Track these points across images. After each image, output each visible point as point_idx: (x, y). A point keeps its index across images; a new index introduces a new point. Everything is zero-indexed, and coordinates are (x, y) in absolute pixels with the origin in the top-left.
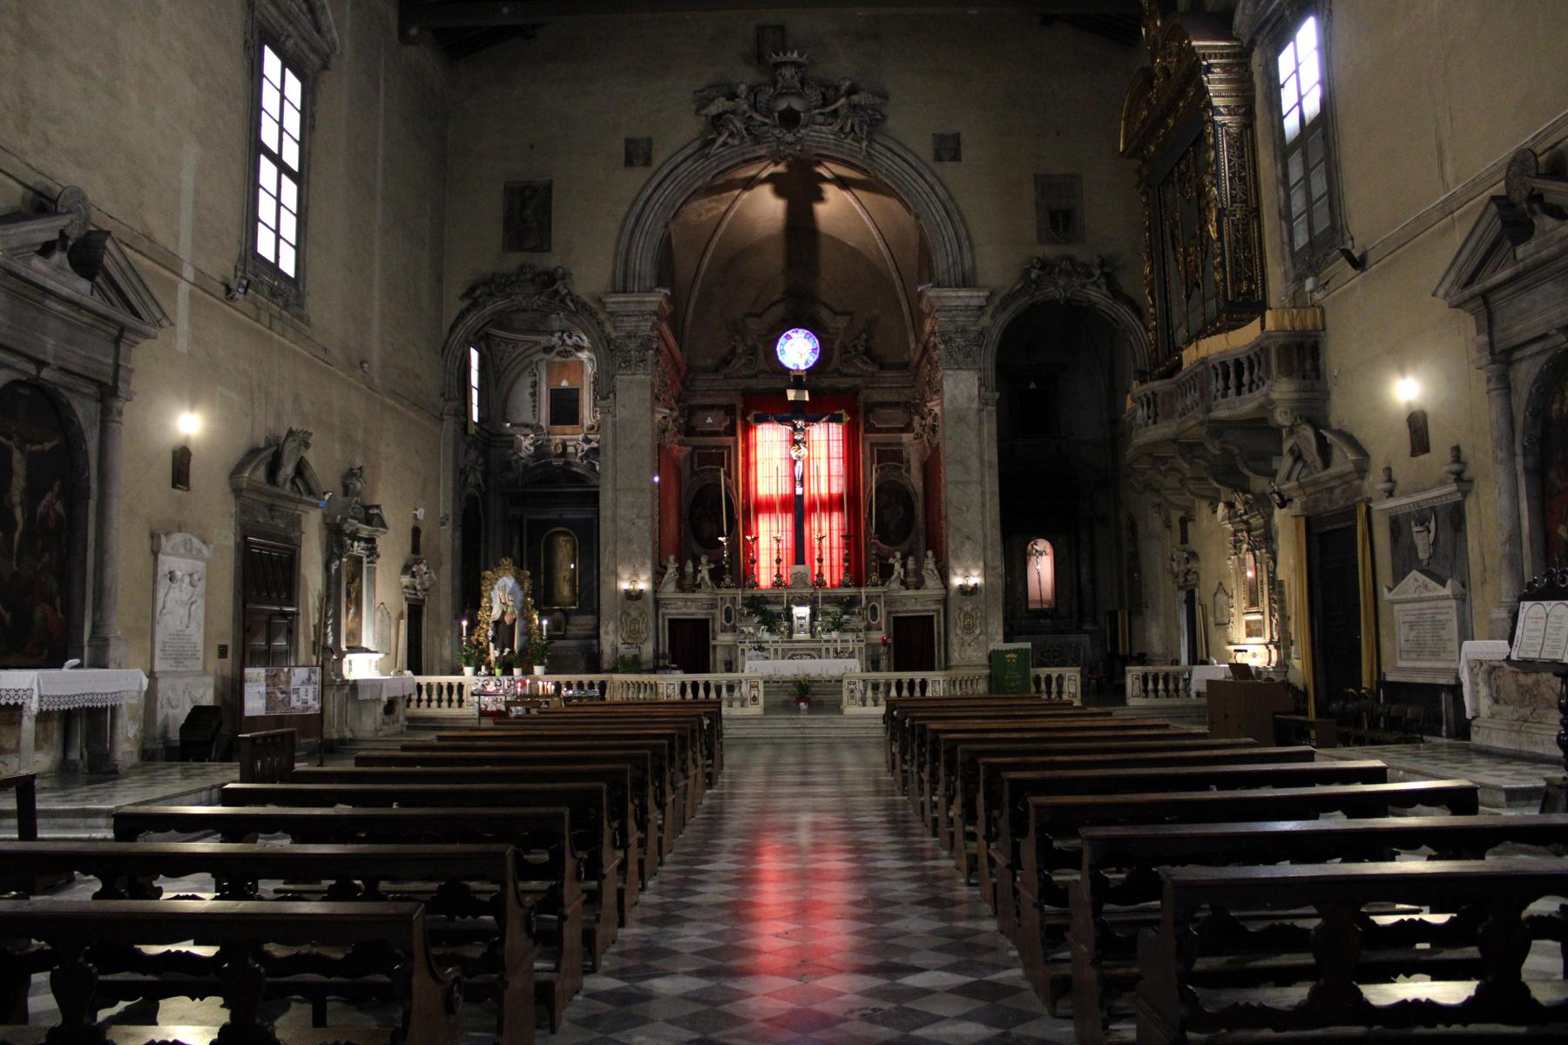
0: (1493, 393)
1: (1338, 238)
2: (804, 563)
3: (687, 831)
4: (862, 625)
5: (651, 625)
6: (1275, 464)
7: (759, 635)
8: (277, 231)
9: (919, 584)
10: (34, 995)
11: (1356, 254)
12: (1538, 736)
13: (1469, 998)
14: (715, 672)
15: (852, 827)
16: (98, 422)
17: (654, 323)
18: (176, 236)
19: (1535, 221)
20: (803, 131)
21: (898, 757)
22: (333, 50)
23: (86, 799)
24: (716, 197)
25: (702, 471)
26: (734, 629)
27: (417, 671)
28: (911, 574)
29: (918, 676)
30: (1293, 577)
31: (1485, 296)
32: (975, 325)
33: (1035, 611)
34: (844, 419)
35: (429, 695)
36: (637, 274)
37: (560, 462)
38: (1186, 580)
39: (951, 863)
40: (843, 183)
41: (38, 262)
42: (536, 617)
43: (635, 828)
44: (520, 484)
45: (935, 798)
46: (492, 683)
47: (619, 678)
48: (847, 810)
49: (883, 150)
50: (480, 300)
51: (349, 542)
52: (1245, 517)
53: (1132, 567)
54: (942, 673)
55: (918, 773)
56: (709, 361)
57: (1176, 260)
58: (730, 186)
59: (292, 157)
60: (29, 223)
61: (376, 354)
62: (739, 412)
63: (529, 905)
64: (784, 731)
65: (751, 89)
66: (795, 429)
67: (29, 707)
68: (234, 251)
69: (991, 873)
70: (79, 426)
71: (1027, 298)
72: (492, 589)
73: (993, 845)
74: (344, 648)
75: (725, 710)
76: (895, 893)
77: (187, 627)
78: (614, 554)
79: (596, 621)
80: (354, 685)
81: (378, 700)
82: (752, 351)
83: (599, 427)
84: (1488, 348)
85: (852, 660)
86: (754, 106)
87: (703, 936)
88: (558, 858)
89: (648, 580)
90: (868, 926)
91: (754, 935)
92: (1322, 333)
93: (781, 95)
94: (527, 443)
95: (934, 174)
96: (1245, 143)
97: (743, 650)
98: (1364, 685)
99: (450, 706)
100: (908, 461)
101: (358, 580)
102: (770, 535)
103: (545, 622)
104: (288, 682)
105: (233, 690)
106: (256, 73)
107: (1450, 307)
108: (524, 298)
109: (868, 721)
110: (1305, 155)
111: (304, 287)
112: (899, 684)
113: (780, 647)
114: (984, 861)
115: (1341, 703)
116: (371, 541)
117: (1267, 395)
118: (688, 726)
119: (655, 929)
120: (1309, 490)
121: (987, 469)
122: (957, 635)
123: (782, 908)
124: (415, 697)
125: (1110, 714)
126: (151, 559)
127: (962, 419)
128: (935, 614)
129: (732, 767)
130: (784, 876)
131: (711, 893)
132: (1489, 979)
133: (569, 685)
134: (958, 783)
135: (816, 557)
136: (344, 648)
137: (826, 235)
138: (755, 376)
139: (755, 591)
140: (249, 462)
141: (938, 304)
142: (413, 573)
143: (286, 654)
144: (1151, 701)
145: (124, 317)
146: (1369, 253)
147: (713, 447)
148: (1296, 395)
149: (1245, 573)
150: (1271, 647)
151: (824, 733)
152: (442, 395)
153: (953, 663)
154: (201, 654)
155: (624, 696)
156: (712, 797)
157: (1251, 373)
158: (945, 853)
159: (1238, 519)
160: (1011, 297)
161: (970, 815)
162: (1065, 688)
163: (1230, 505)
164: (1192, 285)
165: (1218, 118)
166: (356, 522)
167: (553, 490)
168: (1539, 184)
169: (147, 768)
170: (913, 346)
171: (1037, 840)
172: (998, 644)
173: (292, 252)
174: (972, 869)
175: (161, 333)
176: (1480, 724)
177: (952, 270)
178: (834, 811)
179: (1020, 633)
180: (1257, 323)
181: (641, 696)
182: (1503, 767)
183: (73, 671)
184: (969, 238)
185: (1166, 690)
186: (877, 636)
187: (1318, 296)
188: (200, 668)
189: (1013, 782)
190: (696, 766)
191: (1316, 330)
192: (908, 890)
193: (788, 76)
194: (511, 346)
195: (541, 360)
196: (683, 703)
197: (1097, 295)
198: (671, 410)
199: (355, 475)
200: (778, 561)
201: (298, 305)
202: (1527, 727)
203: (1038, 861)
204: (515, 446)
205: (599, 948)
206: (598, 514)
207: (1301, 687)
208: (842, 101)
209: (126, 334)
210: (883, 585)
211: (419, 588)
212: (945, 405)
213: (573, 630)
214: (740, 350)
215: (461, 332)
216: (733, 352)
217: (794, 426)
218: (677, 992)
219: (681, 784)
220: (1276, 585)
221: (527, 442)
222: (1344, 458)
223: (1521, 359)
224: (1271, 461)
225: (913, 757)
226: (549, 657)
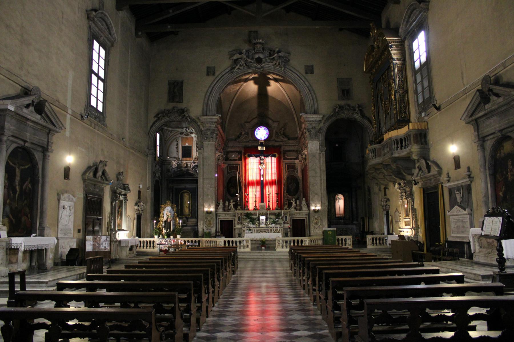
0: (479, 150)
1: (432, 100)
2: (264, 202)
3: (227, 288)
4: (282, 222)
5: (215, 222)
6: (413, 172)
7: (249, 225)
8: (97, 98)
9: (301, 209)
10: (35, 337)
11: (437, 106)
12: (493, 258)
13: (452, 336)
14: (235, 237)
15: (279, 287)
16: (42, 160)
17: (216, 125)
18: (66, 100)
19: (491, 98)
20: (263, 64)
21: (293, 265)
22: (115, 41)
23: (39, 278)
24: (236, 85)
25: (231, 172)
26: (241, 223)
27: (140, 237)
28: (298, 206)
29: (300, 239)
30: (419, 207)
31: (476, 120)
32: (318, 126)
33: (338, 217)
34: (277, 156)
35: (144, 245)
36: (210, 110)
37: (185, 169)
38: (386, 208)
39: (309, 298)
40: (276, 80)
41: (25, 110)
42: (178, 219)
43: (211, 288)
44: (172, 176)
45: (304, 278)
46: (164, 241)
47: (204, 239)
48: (277, 282)
49: (289, 71)
50: (160, 118)
51: (119, 196)
52: (404, 188)
53: (369, 203)
54: (308, 238)
55: (299, 270)
56: (233, 137)
57: (382, 106)
58: (240, 81)
59: (102, 74)
60: (23, 98)
61: (127, 136)
62: (243, 153)
63: (182, 310)
64: (257, 256)
65: (247, 51)
66: (261, 159)
67: (21, 249)
68: (83, 104)
69: (320, 301)
70: (36, 160)
71: (335, 118)
72: (164, 210)
73: (320, 293)
74: (117, 229)
75: (238, 250)
76: (291, 308)
77: (68, 223)
78: (203, 200)
79: (197, 220)
80: (120, 242)
81: (127, 246)
82: (247, 134)
83: (198, 158)
84: (477, 136)
85: (279, 233)
86: (248, 57)
87: (232, 320)
88: (189, 297)
89: (214, 208)
90: (283, 317)
91: (248, 320)
92: (427, 130)
93: (256, 53)
94: (175, 163)
95: (305, 78)
96: (403, 70)
97: (244, 230)
98: (441, 242)
99: (150, 248)
100: (297, 169)
101: (121, 208)
102: (253, 192)
103: (181, 221)
104: (100, 241)
105: (82, 243)
106: (91, 48)
107: (466, 123)
108: (174, 117)
109: (284, 253)
110: (421, 74)
111: (105, 115)
112: (294, 241)
113: (256, 229)
114: (318, 298)
115: (434, 247)
116: (125, 195)
117: (410, 150)
118: (227, 255)
119: (218, 318)
120: (424, 180)
121: (322, 172)
122: (313, 225)
123: (256, 312)
124: (139, 245)
125: (359, 251)
126: (57, 202)
127: (314, 156)
128: (306, 218)
129: (240, 268)
130: (257, 302)
131: (234, 307)
132: (458, 331)
133: (188, 242)
134: (311, 274)
135: (268, 200)
136: (117, 229)
137: (271, 97)
138: (248, 142)
139: (248, 211)
140: (88, 171)
141: (306, 119)
142: (139, 205)
143: (98, 232)
144: (375, 246)
145: (51, 126)
146: (441, 106)
147: (234, 165)
148: (419, 150)
149: (404, 205)
150: (413, 229)
151: (270, 257)
152: (148, 148)
153: (311, 234)
154: (72, 232)
155: (206, 245)
156: (234, 278)
157: (405, 142)
158: (307, 295)
159: (402, 188)
160: (330, 117)
161: (314, 284)
162: (347, 242)
163: (399, 184)
164: (387, 114)
165: (394, 62)
166: (121, 189)
167: (182, 178)
168: (491, 87)
169: (56, 268)
170: (299, 132)
171: (332, 291)
172: (326, 228)
173: (92, 93)
174: (315, 300)
175: (62, 131)
176: (477, 254)
177: (311, 109)
178: (272, 282)
179: (333, 225)
180: (407, 126)
181: (211, 245)
182: (481, 268)
183: (34, 237)
184: (316, 98)
185: (380, 243)
186: (287, 226)
187: (426, 118)
188: (72, 236)
189: (326, 274)
190: (229, 268)
191: (425, 129)
192: (295, 307)
193: (259, 47)
194: (170, 132)
195: (179, 137)
196: (225, 247)
197: (357, 116)
198: (221, 153)
199: (120, 174)
200: (255, 201)
201: (103, 121)
202: (490, 255)
203: (332, 298)
204: (171, 164)
205: (201, 324)
206: (198, 186)
207: (422, 242)
208: (276, 55)
209: (51, 132)
210: (289, 209)
211: (140, 210)
212: (309, 151)
213: (189, 223)
214: (243, 133)
215: (154, 128)
216: (241, 134)
217: (260, 158)
218: (225, 337)
219: (225, 273)
220: (414, 210)
221: (175, 163)
222: (434, 170)
223: (487, 140)
224: (412, 170)
225: (297, 265)
226: (182, 232)
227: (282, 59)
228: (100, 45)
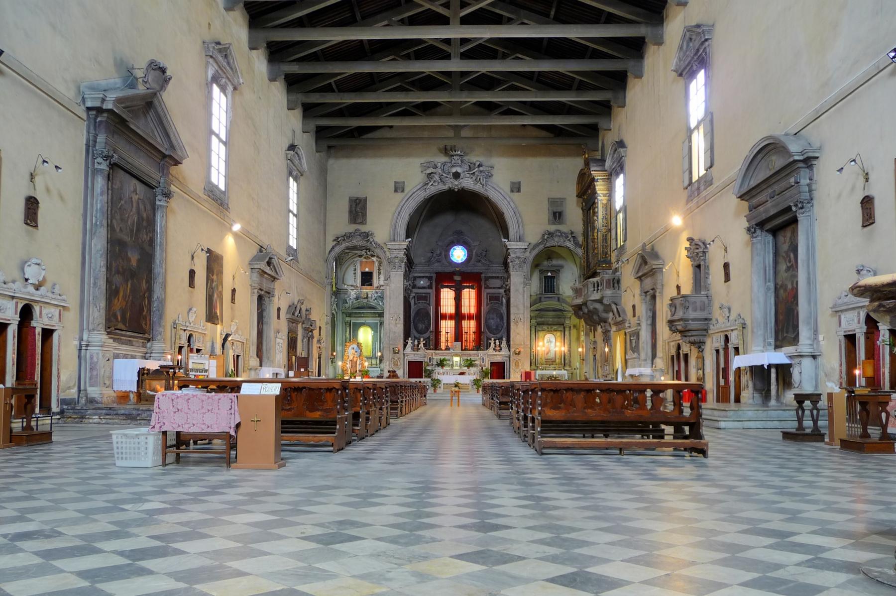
49: (491, 188)
94: (353, 294)
193: (456, 159)
227: (484, 174)
228: (294, 180)
